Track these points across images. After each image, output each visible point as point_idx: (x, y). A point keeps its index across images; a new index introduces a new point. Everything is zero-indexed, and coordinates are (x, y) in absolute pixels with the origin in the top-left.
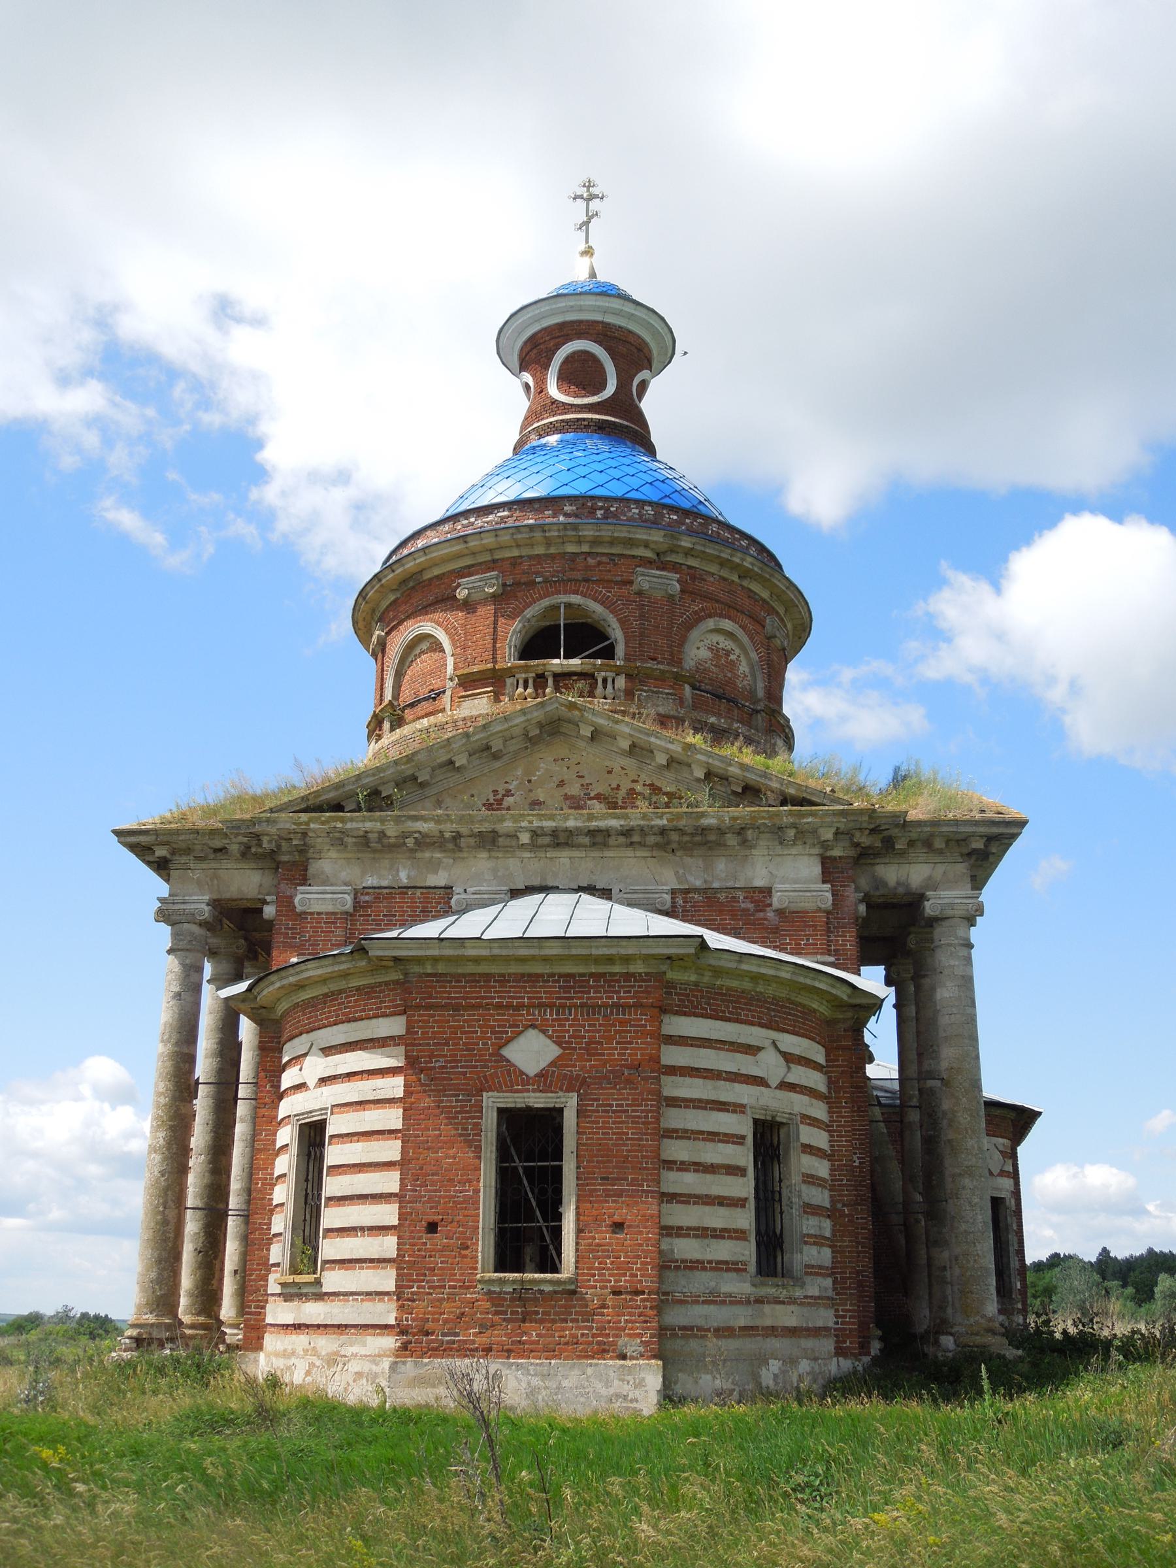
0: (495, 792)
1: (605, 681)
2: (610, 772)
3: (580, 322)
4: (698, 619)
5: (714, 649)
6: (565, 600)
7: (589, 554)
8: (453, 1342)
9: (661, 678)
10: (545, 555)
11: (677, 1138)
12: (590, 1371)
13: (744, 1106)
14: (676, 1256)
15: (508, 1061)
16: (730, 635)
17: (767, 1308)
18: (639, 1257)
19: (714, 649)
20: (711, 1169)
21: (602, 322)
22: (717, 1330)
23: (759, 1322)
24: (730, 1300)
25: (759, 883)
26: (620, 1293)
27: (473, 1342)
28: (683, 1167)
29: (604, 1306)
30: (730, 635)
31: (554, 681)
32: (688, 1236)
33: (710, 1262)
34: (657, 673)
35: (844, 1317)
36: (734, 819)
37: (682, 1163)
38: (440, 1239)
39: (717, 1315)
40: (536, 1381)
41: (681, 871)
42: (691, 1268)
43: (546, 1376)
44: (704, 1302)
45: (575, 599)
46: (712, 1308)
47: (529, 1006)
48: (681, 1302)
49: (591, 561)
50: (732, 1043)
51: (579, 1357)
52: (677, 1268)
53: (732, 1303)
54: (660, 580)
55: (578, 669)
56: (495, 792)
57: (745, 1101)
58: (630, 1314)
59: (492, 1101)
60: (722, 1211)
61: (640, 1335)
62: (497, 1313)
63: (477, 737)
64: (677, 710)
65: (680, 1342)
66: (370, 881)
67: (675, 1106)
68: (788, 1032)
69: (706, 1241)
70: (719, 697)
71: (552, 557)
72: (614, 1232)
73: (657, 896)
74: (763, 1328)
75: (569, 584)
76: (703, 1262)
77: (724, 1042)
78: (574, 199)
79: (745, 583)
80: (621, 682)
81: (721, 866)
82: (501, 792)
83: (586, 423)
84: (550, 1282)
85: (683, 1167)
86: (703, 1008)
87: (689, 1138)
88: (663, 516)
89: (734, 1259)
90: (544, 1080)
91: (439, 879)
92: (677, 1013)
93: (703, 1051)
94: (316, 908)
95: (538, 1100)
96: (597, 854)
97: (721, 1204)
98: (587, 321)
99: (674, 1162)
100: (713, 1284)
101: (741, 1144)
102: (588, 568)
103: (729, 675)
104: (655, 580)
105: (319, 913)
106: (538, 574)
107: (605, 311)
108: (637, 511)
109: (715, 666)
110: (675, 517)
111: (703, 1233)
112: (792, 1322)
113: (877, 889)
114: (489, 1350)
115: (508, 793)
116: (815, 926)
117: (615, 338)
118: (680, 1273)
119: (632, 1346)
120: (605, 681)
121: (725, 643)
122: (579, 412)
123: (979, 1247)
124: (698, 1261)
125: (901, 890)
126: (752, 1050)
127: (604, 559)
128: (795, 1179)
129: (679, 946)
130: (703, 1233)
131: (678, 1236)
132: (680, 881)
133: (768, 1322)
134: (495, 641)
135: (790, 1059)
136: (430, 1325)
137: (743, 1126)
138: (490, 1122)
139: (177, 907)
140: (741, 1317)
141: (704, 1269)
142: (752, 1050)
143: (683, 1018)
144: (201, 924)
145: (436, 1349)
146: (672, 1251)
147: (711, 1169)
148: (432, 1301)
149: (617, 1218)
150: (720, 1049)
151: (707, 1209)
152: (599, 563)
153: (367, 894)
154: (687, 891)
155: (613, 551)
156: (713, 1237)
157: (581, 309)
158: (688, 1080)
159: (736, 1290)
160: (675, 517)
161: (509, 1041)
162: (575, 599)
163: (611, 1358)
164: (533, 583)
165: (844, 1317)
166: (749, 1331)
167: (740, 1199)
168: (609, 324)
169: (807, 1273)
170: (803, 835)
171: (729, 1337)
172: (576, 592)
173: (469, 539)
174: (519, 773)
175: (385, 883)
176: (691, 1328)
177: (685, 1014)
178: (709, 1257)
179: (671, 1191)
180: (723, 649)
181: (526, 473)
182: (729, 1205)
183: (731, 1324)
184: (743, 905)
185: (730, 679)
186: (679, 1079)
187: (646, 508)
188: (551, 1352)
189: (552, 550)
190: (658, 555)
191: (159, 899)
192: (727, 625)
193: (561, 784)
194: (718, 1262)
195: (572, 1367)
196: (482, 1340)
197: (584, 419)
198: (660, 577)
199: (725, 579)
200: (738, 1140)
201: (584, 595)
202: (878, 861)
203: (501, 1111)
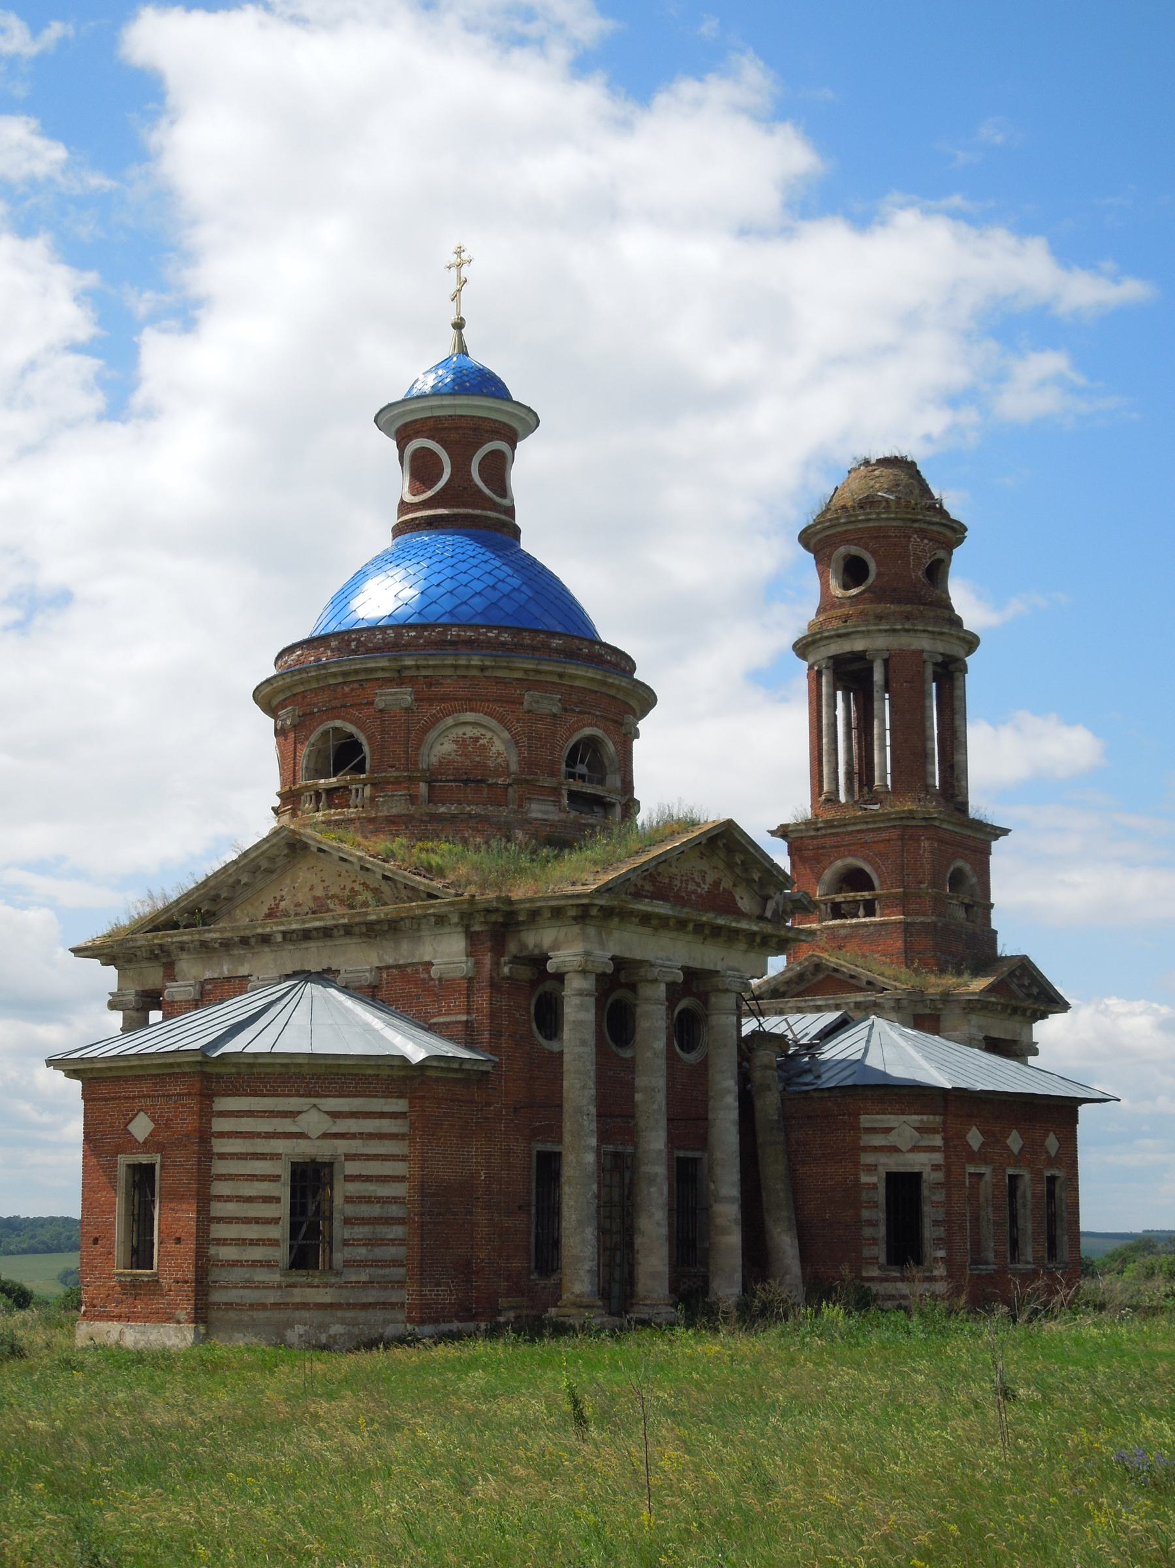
0: (275, 898)
1: (357, 790)
2: (340, 876)
3: (416, 421)
4: (435, 720)
5: (461, 743)
6: (332, 725)
7: (345, 683)
8: (105, 1312)
9: (397, 782)
10: (318, 688)
11: (225, 1180)
12: (162, 1330)
13: (281, 1154)
14: (221, 1258)
15: (130, 1133)
16: (475, 724)
17: (296, 1291)
18: (186, 1259)
19: (461, 743)
20: (250, 1199)
21: (432, 417)
22: (251, 1305)
23: (288, 1300)
24: (265, 1286)
25: (427, 959)
26: (178, 1282)
27: (113, 1312)
28: (229, 1199)
29: (170, 1291)
30: (475, 724)
31: (327, 798)
32: (230, 1244)
33: (248, 1261)
34: (392, 780)
35: (412, 1295)
36: (386, 914)
37: (228, 1196)
38: (99, 1249)
39: (250, 1296)
40: (138, 1336)
41: (381, 952)
42: (233, 1266)
43: (143, 1333)
44: (241, 1287)
45: (338, 723)
46: (246, 1292)
47: (139, 1097)
48: (226, 1287)
49: (347, 689)
50: (272, 1112)
51: (159, 1322)
52: (223, 1265)
53: (264, 1288)
54: (394, 697)
55: (337, 785)
56: (275, 898)
57: (280, 1152)
58: (182, 1295)
59: (123, 1160)
60: (256, 1227)
61: (186, 1309)
62: (124, 1294)
63: (242, 863)
64: (408, 809)
65: (221, 1313)
66: (208, 975)
67: (223, 1159)
68: (329, 1096)
69: (243, 1248)
70: (466, 782)
71: (322, 688)
72: (176, 1244)
73: (362, 974)
74: (293, 1304)
75: (333, 712)
76: (241, 1261)
77: (265, 1112)
78: (449, 268)
79: (487, 674)
80: (368, 791)
81: (405, 946)
82: (279, 898)
83: (417, 522)
84: (147, 1275)
85: (229, 1199)
86: (244, 1090)
87: (233, 1180)
88: (402, 635)
89: (267, 1258)
90: (149, 1145)
91: (243, 971)
92: (223, 1095)
93: (244, 1120)
94: (177, 998)
95: (144, 1159)
96: (330, 943)
97: (257, 1223)
98: (422, 419)
99: (223, 1196)
100: (247, 1276)
101: (278, 1181)
102: (345, 696)
103: (478, 759)
104: (391, 698)
105: (181, 1002)
106: (315, 705)
107: (431, 408)
108: (380, 636)
109: (460, 755)
110: (413, 634)
111: (241, 1242)
112: (328, 1299)
113: (521, 951)
114: (121, 1316)
115: (282, 899)
116: (460, 991)
117: (446, 428)
118: (223, 1269)
119: (182, 1315)
120: (357, 790)
121: (471, 732)
122: (416, 510)
123: (571, 1240)
124: (237, 1261)
125: (536, 952)
126: (292, 1114)
127: (356, 686)
128: (338, 1201)
129: (193, 1056)
130: (241, 1242)
131: (224, 1245)
132: (380, 961)
133: (298, 1300)
134: (295, 766)
135: (335, 1115)
136: (95, 1301)
137: (282, 1169)
138: (122, 1172)
139: (121, 998)
140: (271, 1297)
141: (242, 1266)
142: (292, 1114)
143: (229, 1098)
144: (133, 1009)
145: (97, 1316)
146: (218, 1254)
147: (250, 1199)
148: (95, 1287)
149: (177, 1235)
150: (261, 1117)
151: (244, 1226)
152: (352, 690)
153: (210, 983)
154: (388, 967)
155: (360, 678)
156: (250, 1245)
157: (412, 411)
158: (231, 1141)
159: (267, 1279)
160: (413, 634)
161: (131, 1120)
162: (338, 723)
163: (173, 1323)
164: (312, 713)
165: (412, 1295)
166: (276, 1306)
167: (273, 1219)
168: (439, 417)
169: (344, 1266)
170: (441, 920)
171: (263, 1309)
172: (338, 718)
173: (272, 682)
174: (288, 881)
175: (216, 976)
176: (231, 1304)
177: (229, 1095)
178: (245, 1258)
179: (218, 1215)
180: (471, 738)
181: (411, 563)
182: (263, 1223)
183: (263, 1301)
184: (422, 976)
185: (479, 762)
186: (225, 1140)
187: (388, 632)
188: (146, 1318)
189: (321, 684)
190: (399, 671)
191: (111, 994)
192: (469, 716)
193: (312, 889)
194: (253, 1261)
195: (154, 1328)
196: (117, 1311)
197: (416, 518)
198: (396, 693)
199: (464, 677)
200: (275, 1178)
201: (344, 720)
202: (521, 928)
203: (128, 1165)
